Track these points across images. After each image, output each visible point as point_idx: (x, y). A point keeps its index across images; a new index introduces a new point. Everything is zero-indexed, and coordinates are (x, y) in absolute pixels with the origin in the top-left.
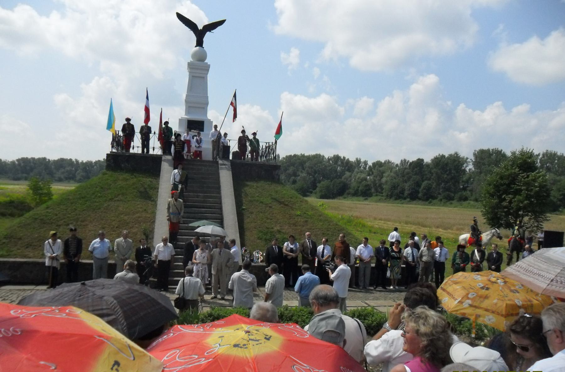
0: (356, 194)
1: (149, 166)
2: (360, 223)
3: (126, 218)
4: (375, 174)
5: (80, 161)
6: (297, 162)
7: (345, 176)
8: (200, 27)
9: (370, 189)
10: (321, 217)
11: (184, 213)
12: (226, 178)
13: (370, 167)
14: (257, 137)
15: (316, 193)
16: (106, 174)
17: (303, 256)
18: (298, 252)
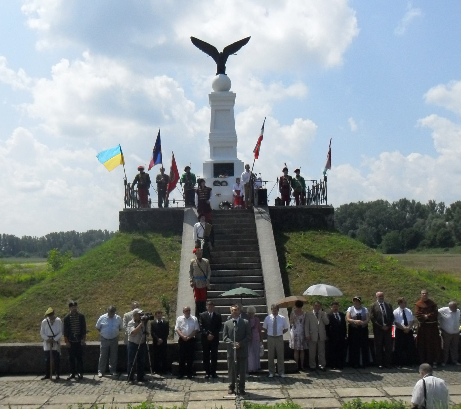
0: (433, 245)
1: (171, 222)
2: (445, 279)
3: (143, 287)
4: (455, 218)
5: (110, 232)
6: (356, 214)
7: (416, 223)
8: (220, 50)
9: (450, 238)
10: (395, 271)
11: (211, 276)
12: (264, 229)
13: (448, 209)
14: (301, 175)
15: (381, 248)
16: (120, 236)
17: (374, 325)
18: (367, 320)
